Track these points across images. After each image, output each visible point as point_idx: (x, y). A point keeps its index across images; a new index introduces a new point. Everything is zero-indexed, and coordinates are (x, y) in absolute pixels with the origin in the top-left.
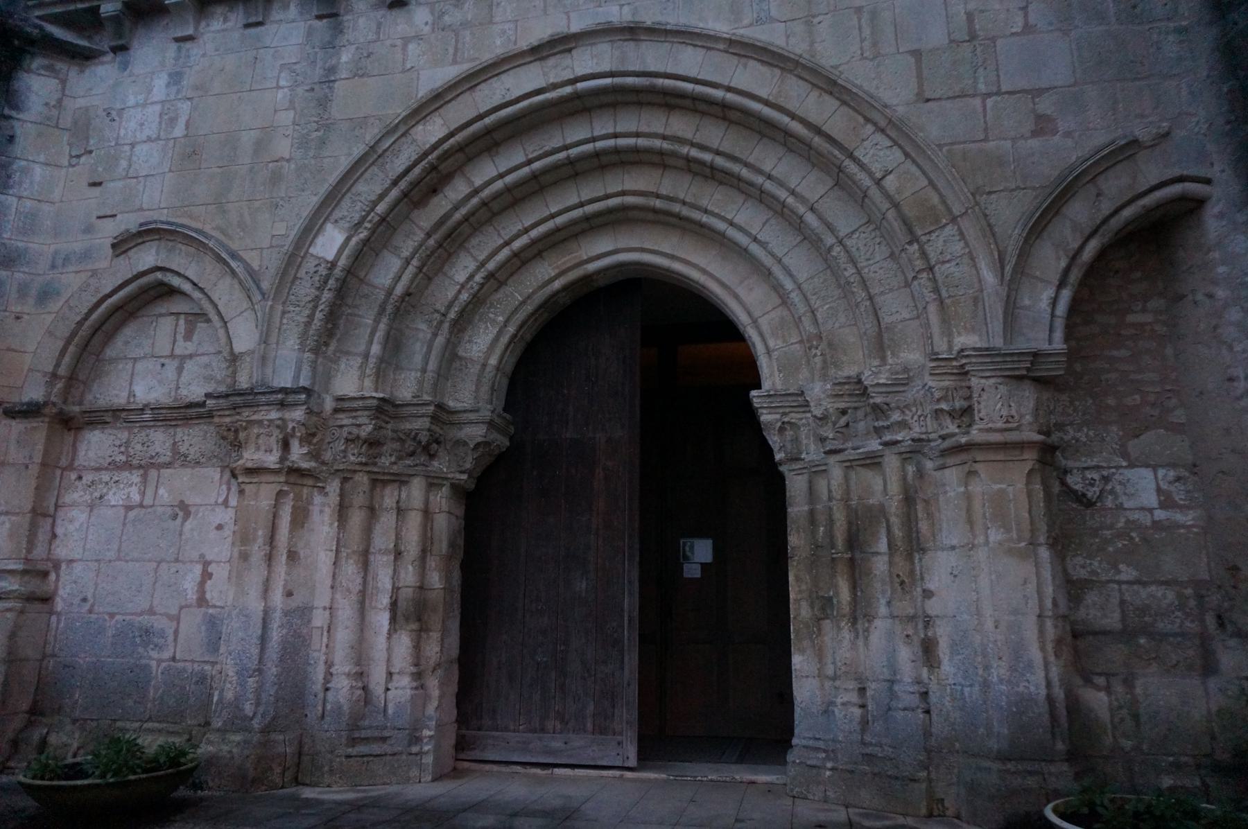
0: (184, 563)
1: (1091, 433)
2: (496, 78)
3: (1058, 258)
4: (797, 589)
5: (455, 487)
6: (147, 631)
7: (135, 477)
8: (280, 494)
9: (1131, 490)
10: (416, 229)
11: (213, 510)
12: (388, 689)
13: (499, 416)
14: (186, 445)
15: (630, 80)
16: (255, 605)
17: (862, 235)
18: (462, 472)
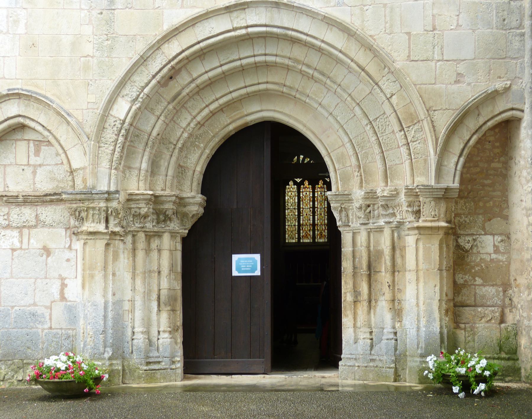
0: (50, 279)
1: (471, 218)
2: (206, 21)
3: (460, 144)
4: (345, 287)
6: (33, 315)
7: (16, 233)
9: (483, 245)
10: (162, 99)
11: (63, 251)
12: (158, 339)
14: (44, 215)
15: (275, 30)
16: (100, 301)
17: (381, 120)
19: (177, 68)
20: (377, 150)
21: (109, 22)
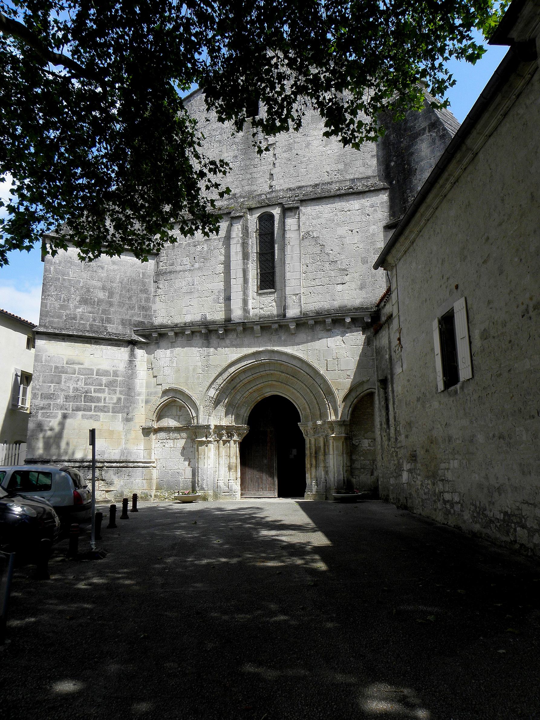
7: (172, 441)
20: (317, 406)
21: (207, 361)
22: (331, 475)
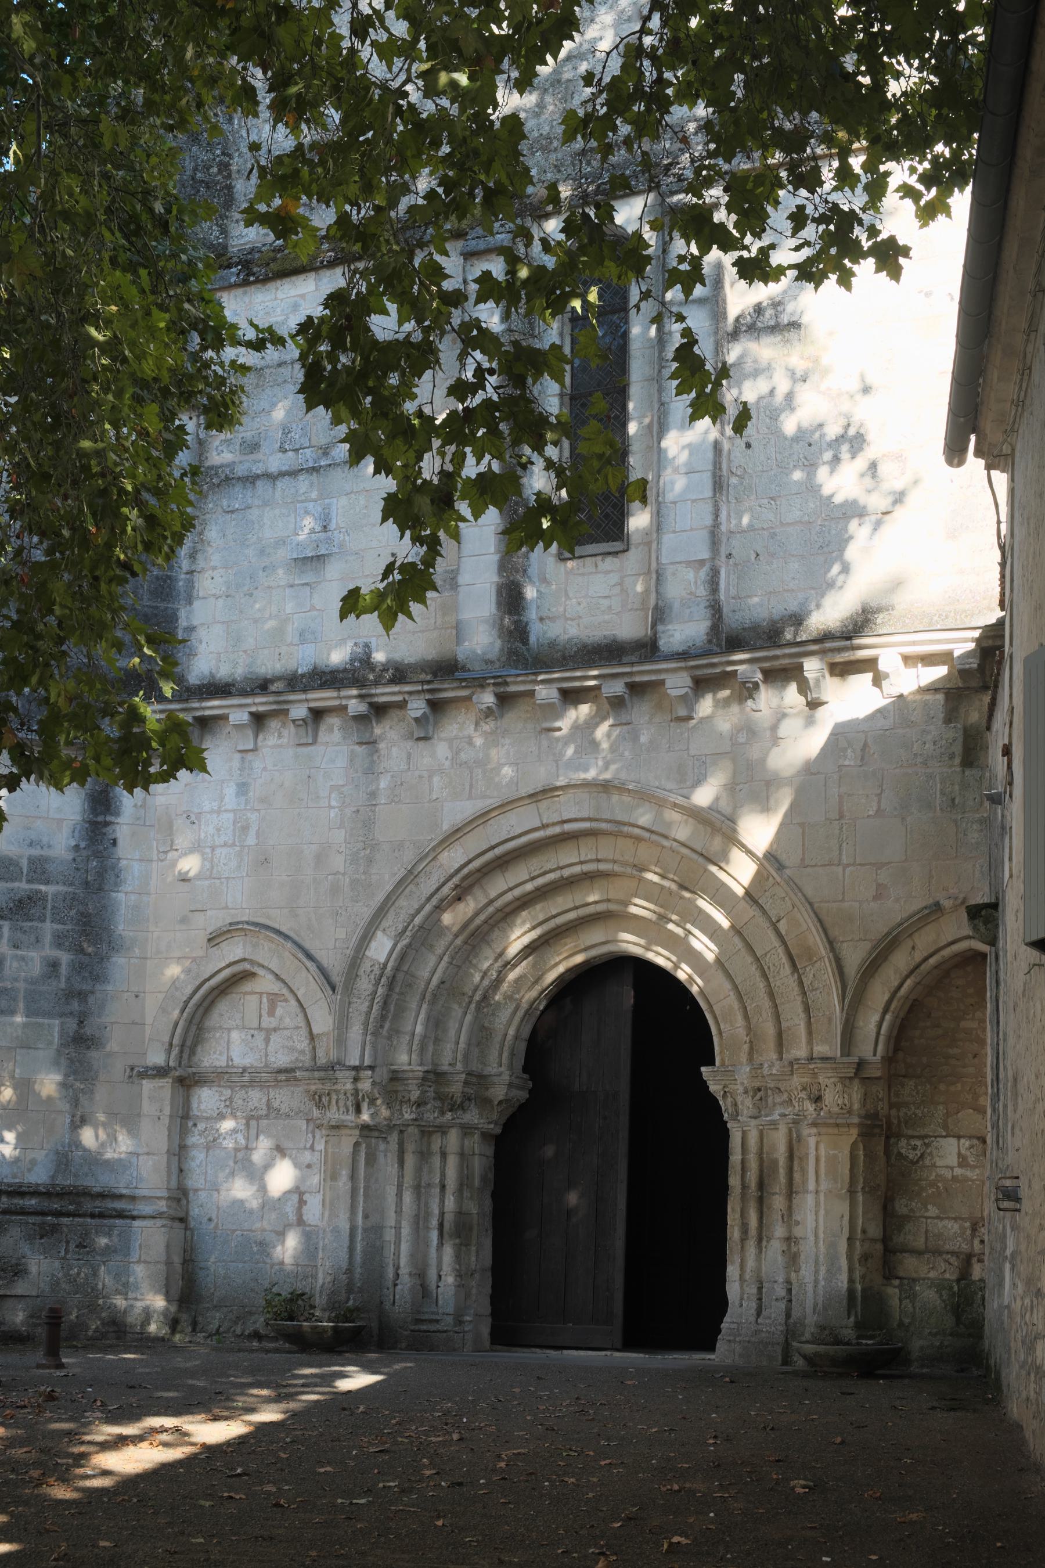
5: (485, 1135)
8: (357, 1145)
13: (517, 1077)
16: (345, 1226)
18: (489, 1123)
19: (465, 884)
21: (368, 824)
22: (806, 1272)
